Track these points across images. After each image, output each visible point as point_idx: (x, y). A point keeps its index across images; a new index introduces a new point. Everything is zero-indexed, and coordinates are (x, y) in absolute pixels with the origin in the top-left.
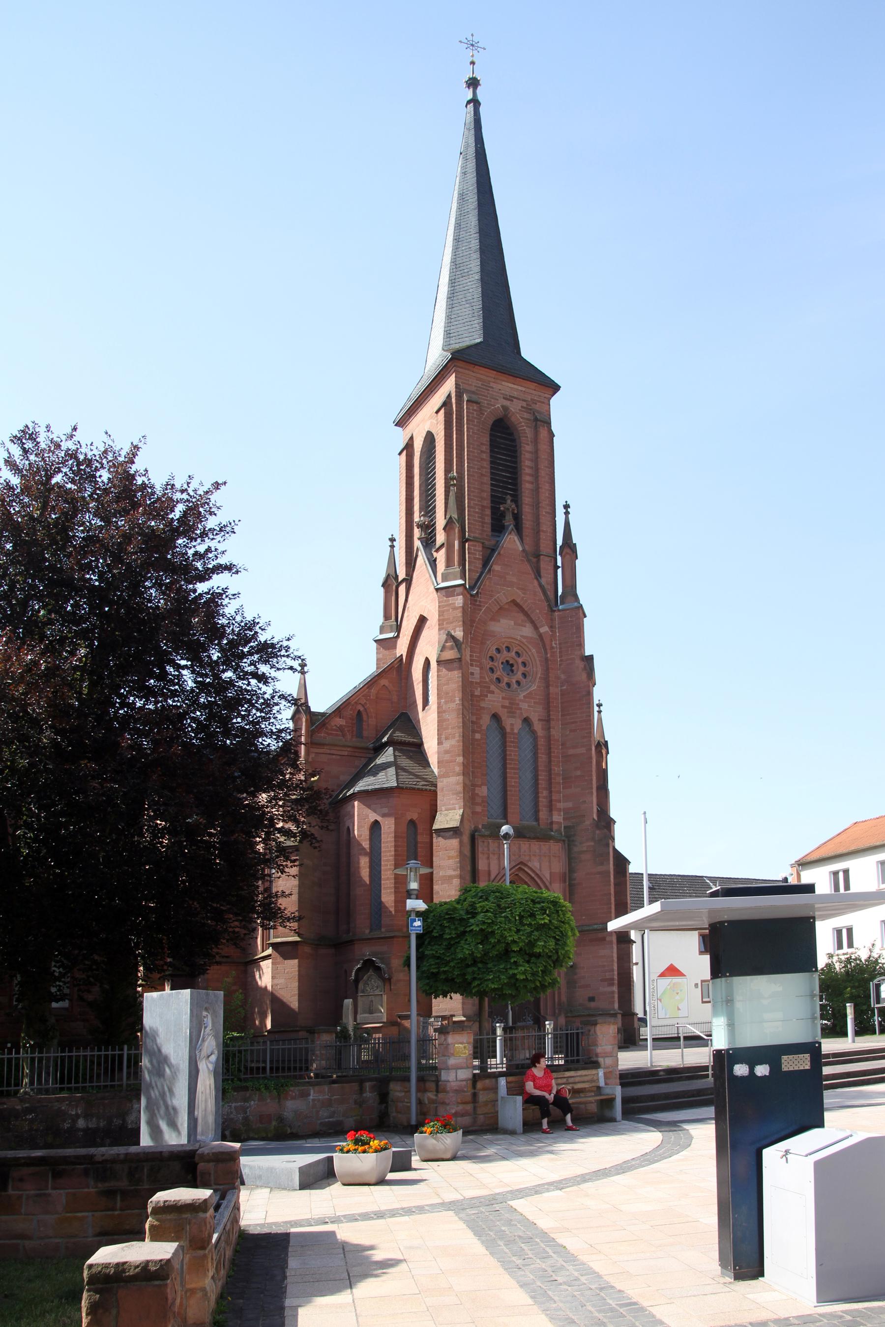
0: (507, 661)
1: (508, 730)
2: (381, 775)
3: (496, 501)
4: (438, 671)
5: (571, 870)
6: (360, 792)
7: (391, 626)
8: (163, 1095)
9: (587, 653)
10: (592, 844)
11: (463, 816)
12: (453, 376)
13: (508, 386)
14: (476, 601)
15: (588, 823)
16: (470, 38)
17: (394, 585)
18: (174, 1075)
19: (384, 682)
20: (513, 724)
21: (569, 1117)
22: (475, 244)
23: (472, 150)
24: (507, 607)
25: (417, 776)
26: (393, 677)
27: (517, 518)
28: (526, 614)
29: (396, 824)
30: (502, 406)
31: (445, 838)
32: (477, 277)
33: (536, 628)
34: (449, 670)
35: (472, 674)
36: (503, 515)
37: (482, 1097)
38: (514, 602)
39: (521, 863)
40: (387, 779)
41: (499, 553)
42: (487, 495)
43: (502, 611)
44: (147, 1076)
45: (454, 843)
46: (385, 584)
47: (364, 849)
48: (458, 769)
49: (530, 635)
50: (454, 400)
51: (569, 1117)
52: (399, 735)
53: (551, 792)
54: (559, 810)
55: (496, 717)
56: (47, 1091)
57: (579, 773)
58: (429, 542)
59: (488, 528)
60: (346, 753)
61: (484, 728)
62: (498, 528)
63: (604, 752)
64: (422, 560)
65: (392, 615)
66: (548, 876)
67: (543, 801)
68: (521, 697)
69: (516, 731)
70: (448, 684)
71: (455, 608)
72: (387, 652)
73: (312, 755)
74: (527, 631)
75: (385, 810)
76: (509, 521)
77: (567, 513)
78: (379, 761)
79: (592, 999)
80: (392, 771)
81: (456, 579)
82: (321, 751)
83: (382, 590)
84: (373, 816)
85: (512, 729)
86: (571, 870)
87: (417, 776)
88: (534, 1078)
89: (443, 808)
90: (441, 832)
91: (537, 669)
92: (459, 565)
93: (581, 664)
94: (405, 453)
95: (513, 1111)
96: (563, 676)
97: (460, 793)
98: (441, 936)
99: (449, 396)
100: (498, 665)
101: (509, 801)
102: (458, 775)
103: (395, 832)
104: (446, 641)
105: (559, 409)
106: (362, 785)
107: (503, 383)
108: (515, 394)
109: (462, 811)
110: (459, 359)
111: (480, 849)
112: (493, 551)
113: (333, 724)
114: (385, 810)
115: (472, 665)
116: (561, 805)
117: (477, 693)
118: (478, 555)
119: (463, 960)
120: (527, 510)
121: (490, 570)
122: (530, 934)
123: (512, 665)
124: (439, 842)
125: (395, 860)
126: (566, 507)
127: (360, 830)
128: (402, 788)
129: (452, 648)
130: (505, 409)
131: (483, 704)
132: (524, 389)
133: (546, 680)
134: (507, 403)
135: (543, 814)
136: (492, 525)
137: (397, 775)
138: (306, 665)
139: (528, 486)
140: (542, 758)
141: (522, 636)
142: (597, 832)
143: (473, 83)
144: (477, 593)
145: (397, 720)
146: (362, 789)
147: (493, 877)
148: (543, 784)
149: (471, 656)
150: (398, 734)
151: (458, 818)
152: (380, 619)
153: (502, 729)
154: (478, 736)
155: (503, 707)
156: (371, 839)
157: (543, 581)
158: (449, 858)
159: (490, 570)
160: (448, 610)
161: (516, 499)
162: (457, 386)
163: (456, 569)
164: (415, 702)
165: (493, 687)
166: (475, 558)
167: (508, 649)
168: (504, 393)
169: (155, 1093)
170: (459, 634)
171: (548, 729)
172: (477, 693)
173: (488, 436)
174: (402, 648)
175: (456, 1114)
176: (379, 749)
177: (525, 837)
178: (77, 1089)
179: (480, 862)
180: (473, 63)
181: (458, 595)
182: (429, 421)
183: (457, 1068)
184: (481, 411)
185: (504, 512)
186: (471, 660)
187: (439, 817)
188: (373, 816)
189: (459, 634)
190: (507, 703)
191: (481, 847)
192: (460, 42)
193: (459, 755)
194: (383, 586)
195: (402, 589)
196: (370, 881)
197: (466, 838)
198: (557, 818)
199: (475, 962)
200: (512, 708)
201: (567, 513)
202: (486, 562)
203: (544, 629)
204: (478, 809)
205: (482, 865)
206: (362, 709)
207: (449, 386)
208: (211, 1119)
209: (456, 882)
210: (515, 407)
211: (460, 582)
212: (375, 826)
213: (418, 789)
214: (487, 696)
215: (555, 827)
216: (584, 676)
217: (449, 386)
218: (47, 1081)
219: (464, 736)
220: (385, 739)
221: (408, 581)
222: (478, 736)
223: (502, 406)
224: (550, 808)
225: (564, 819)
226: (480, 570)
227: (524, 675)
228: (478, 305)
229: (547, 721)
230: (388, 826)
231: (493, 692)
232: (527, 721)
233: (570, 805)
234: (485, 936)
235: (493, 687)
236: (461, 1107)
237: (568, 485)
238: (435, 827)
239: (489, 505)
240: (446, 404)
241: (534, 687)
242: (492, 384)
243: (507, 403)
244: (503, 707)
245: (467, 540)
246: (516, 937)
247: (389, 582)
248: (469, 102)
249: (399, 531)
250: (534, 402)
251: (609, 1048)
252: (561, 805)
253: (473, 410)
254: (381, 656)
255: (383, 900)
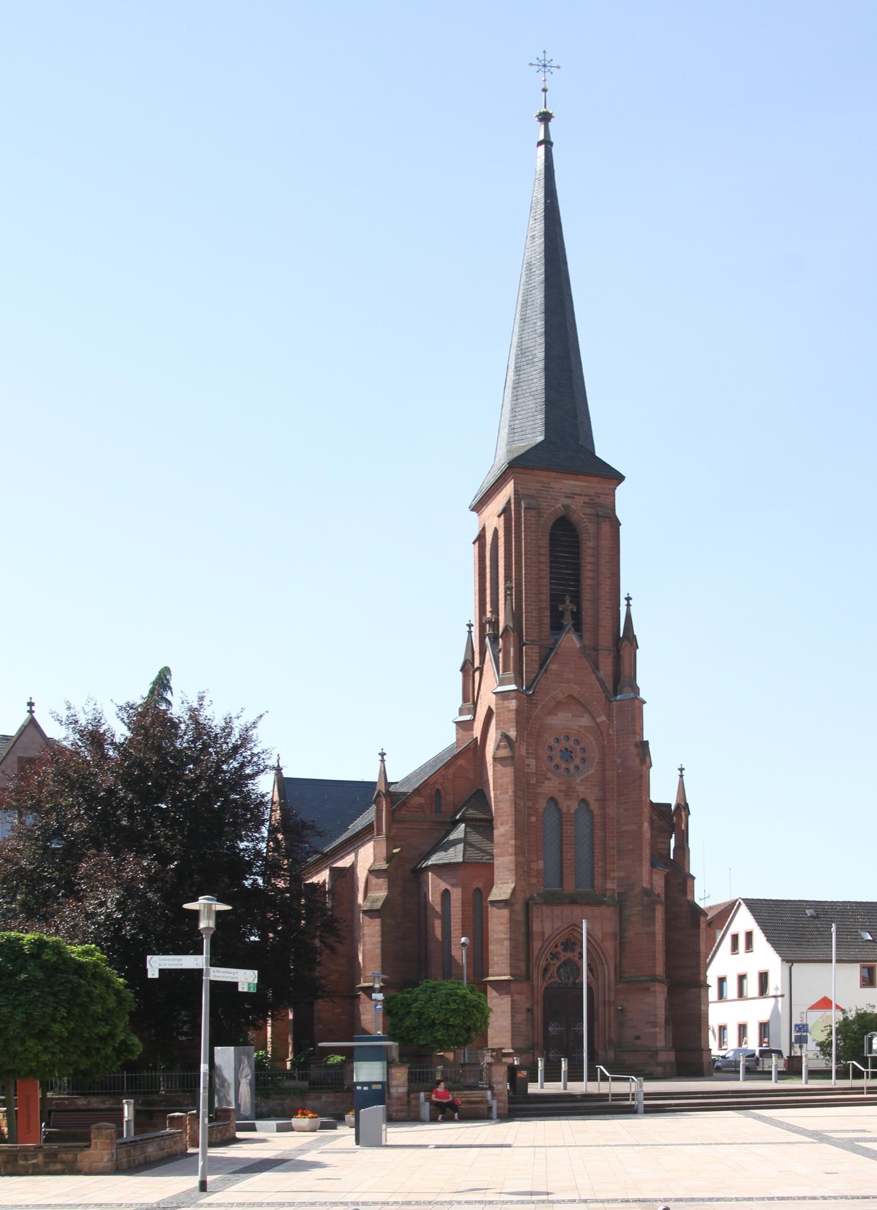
0: (566, 749)
1: (565, 811)
2: (451, 851)
3: (556, 599)
4: (494, 767)
5: (622, 930)
6: (432, 865)
7: (469, 709)
8: (225, 1096)
9: (645, 739)
10: (641, 908)
11: (514, 890)
12: (512, 481)
13: (570, 484)
14: (532, 700)
15: (638, 890)
16: (541, 57)
17: (469, 670)
18: (229, 1087)
19: (461, 762)
20: (570, 805)
21: (456, 1115)
22: (540, 325)
23: (541, 207)
24: (565, 701)
25: (483, 851)
26: (467, 757)
27: (577, 617)
28: (583, 706)
29: (463, 892)
30: (563, 506)
31: (498, 908)
32: (541, 365)
33: (594, 718)
34: (503, 766)
35: (528, 765)
36: (562, 614)
37: (413, 1102)
38: (571, 696)
39: (574, 925)
40: (455, 855)
41: (556, 653)
42: (546, 597)
43: (559, 705)
44: (218, 1086)
45: (505, 912)
46: (463, 669)
47: (437, 912)
48: (511, 850)
49: (588, 724)
50: (512, 506)
51: (456, 1115)
52: (472, 813)
53: (605, 863)
54: (614, 879)
55: (553, 800)
56: (172, 1092)
57: (631, 847)
58: (495, 639)
59: (546, 629)
60: (426, 827)
61: (541, 810)
62: (557, 626)
63: (683, 814)
64: (489, 655)
65: (470, 698)
66: (600, 936)
67: (598, 870)
68: (578, 780)
69: (572, 811)
70: (502, 778)
71: (510, 711)
72: (465, 733)
73: (393, 832)
74: (585, 721)
75: (454, 881)
76: (568, 621)
77: (628, 605)
78: (452, 837)
79: (638, 1038)
80: (460, 847)
81: (510, 684)
82: (404, 826)
83: (461, 674)
84: (444, 886)
85: (569, 810)
86: (622, 930)
87: (483, 851)
88: (437, 1093)
89: (499, 882)
90: (494, 903)
91: (595, 755)
92: (515, 670)
93: (633, 750)
94: (477, 543)
95: (426, 1110)
96: (619, 761)
97: (511, 870)
98: (397, 1013)
99: (509, 502)
100: (556, 754)
101: (565, 872)
102: (511, 855)
103: (463, 899)
104: (500, 741)
105: (625, 501)
106: (436, 859)
107: (565, 481)
108: (578, 490)
109: (513, 885)
110: (519, 466)
111: (534, 914)
112: (552, 650)
113: (412, 802)
114: (454, 881)
115: (528, 758)
116: (615, 874)
117: (533, 781)
118: (535, 657)
119: (407, 1027)
120: (586, 605)
121: (546, 670)
122: (445, 1014)
123: (571, 752)
124: (493, 911)
125: (463, 922)
126: (628, 599)
127: (433, 897)
128: (467, 863)
129: (505, 747)
130: (566, 507)
131: (540, 790)
132: (586, 484)
133: (602, 764)
134: (567, 501)
135: (598, 883)
136: (552, 623)
137: (465, 851)
138: (385, 754)
139: (589, 582)
140: (598, 833)
141: (580, 727)
142: (646, 898)
143: (545, 118)
144: (533, 693)
145: (471, 797)
146: (437, 862)
147: (546, 936)
148: (598, 856)
149: (527, 749)
150: (471, 811)
151: (509, 891)
152: (459, 702)
153: (559, 811)
154: (533, 819)
155: (560, 791)
156: (443, 904)
157: (601, 674)
158: (502, 924)
159: (546, 670)
160: (503, 712)
161: (577, 600)
162: (516, 492)
163: (511, 674)
164: (488, 781)
165: (549, 775)
166: (532, 660)
167: (567, 738)
168: (565, 491)
169: (221, 1095)
170: (513, 733)
171: (603, 807)
172: (533, 781)
173: (548, 538)
174: (477, 732)
175: (397, 1111)
176: (455, 824)
177: (577, 903)
178: (188, 1092)
179: (534, 924)
180: (545, 90)
181: (512, 699)
182: (492, 518)
183: (397, 1086)
184: (540, 515)
185: (562, 612)
186: (527, 753)
187: (495, 890)
188: (444, 886)
189: (513, 733)
190: (563, 788)
191: (535, 912)
192: (531, 64)
193: (511, 839)
194: (461, 670)
195: (477, 674)
196: (443, 938)
197: (519, 907)
198: (611, 885)
199: (414, 1029)
200: (568, 792)
201: (628, 605)
202: (543, 663)
203: (602, 718)
204: (534, 881)
205: (536, 927)
206: (440, 787)
207: (508, 490)
208: (249, 1105)
209: (507, 943)
210: (577, 505)
211: (513, 687)
212: (446, 894)
213: (483, 863)
214: (543, 783)
215: (608, 893)
216: (637, 761)
217: (508, 490)
218: (172, 1087)
219: (516, 822)
220: (458, 817)
221: (481, 669)
222: (533, 819)
223: (563, 506)
224: (605, 876)
225: (618, 886)
226: (537, 671)
227: (584, 760)
228: (541, 397)
229: (603, 801)
230: (456, 894)
231: (549, 779)
232: (584, 801)
233: (622, 874)
234: (420, 1014)
235: (549, 775)
236: (400, 1107)
237: (632, 579)
238: (490, 898)
239: (549, 606)
240: (506, 511)
241: (591, 771)
242: (553, 485)
243: (567, 501)
244: (560, 791)
245: (524, 644)
246: (437, 1016)
247: (467, 667)
248: (540, 144)
249: (475, 620)
250: (598, 495)
251: (500, 1079)
252: (615, 874)
253: (531, 516)
254: (460, 736)
255: (453, 954)
